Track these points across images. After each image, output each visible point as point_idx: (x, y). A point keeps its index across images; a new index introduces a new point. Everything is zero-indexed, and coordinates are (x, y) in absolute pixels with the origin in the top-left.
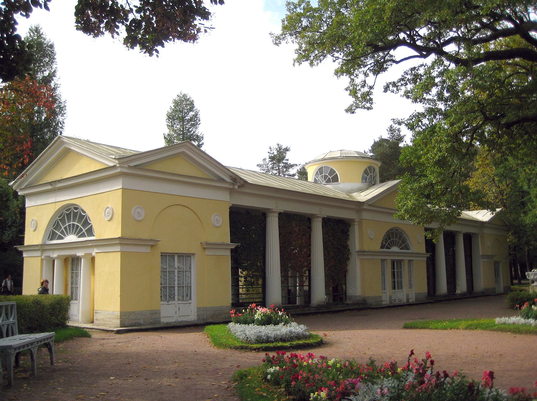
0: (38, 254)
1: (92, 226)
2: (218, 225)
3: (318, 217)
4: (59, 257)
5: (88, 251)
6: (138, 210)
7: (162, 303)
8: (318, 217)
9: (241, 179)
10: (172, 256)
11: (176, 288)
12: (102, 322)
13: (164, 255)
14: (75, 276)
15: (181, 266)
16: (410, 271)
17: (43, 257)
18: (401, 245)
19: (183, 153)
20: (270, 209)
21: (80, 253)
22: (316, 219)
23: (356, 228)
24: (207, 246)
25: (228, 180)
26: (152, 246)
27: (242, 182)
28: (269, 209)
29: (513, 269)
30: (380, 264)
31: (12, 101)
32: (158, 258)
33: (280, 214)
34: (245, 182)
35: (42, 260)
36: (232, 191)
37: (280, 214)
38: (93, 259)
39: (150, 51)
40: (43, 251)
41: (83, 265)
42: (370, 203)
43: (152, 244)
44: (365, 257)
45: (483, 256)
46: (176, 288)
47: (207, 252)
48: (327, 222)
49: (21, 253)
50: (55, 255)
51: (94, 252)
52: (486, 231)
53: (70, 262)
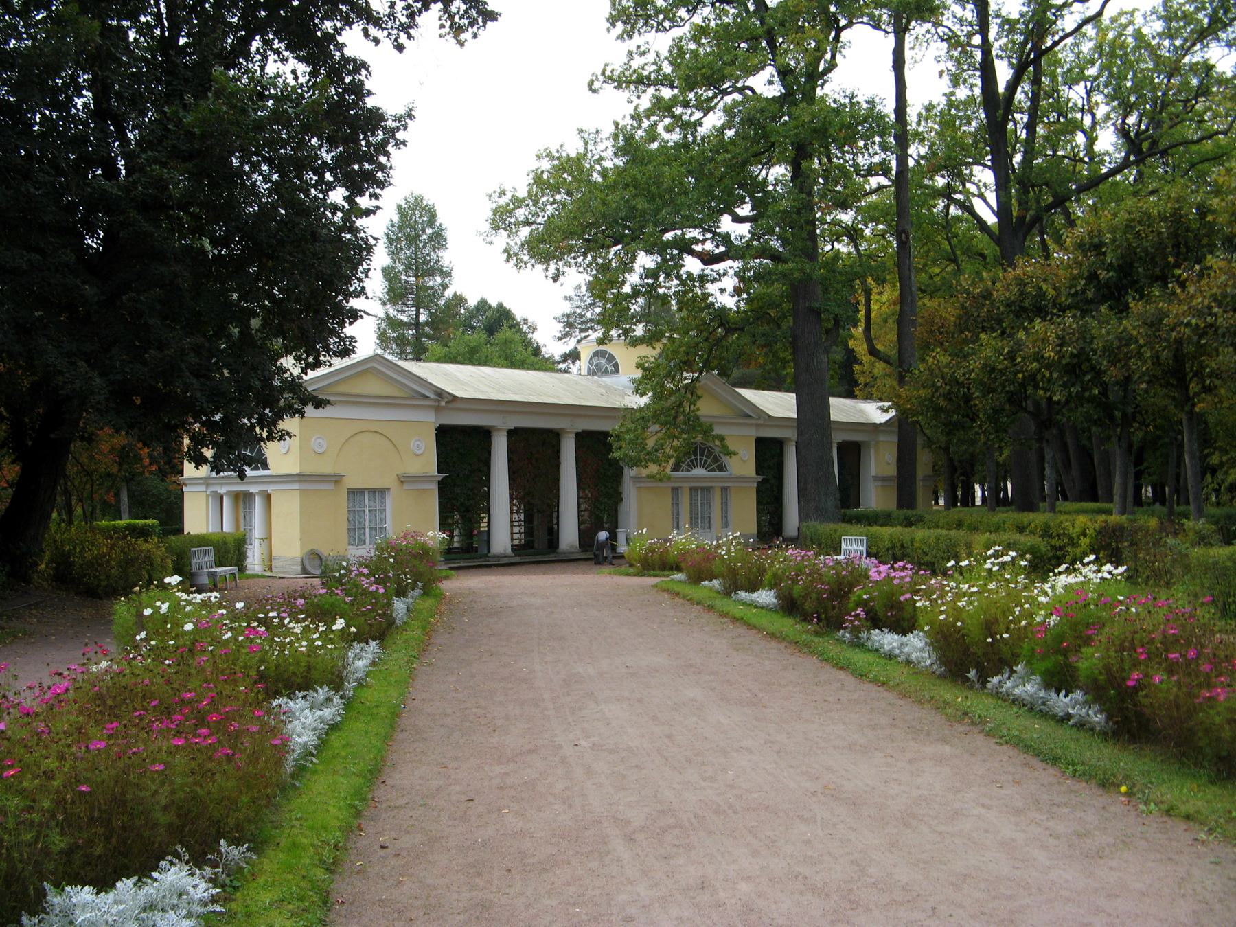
0: (203, 488)
2: (419, 452)
3: (499, 430)
4: (229, 493)
6: (320, 441)
7: (350, 547)
8: (499, 430)
9: (449, 393)
10: (361, 492)
11: (367, 530)
12: (281, 569)
13: (351, 492)
14: (248, 516)
15: (372, 503)
16: (725, 505)
17: (209, 493)
19: (373, 368)
21: (253, 489)
23: (872, 451)
24: (404, 480)
25: (432, 396)
26: (336, 482)
27: (451, 398)
28: (563, 430)
29: (959, 493)
30: (670, 495)
31: (340, 214)
32: (344, 495)
33: (577, 435)
34: (454, 396)
35: (207, 496)
36: (438, 409)
37: (577, 435)
38: (269, 497)
39: (419, 200)
40: (208, 485)
41: (258, 502)
43: (336, 479)
44: (643, 485)
45: (876, 478)
46: (367, 530)
47: (406, 486)
48: (514, 435)
49: (180, 486)
50: (222, 490)
51: (270, 488)
52: (882, 438)
53: (241, 498)
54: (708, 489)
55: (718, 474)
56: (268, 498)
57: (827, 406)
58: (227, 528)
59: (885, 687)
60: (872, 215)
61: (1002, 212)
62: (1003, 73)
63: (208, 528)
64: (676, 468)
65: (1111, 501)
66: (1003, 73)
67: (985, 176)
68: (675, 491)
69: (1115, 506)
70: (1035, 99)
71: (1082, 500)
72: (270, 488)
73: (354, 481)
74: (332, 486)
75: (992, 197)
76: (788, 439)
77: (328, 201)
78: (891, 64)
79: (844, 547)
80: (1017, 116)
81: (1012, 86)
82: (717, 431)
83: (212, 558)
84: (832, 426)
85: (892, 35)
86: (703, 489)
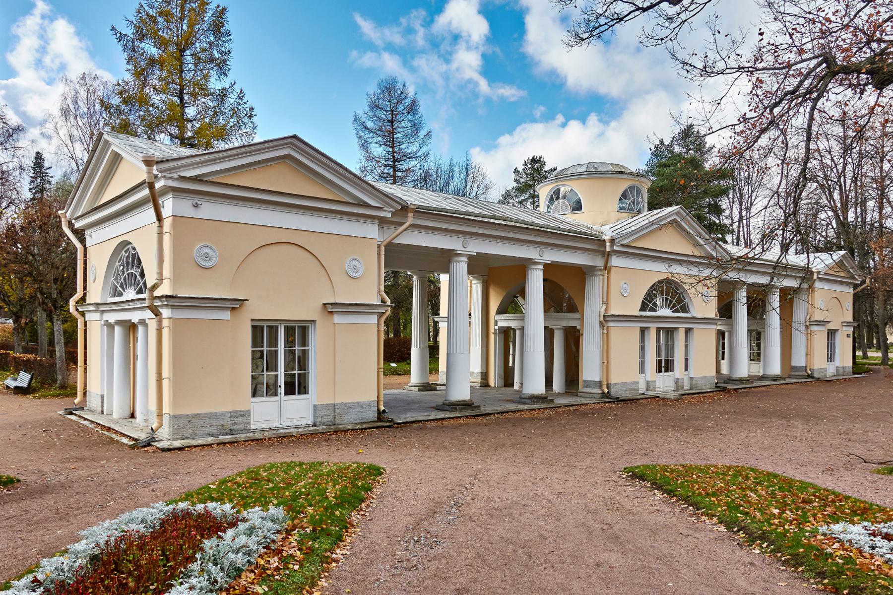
2: (353, 275)
3: (537, 263)
18: (674, 306)
20: (454, 250)
37: (471, 258)
42: (624, 242)
47: (337, 319)
68: (110, 326)
74: (226, 315)
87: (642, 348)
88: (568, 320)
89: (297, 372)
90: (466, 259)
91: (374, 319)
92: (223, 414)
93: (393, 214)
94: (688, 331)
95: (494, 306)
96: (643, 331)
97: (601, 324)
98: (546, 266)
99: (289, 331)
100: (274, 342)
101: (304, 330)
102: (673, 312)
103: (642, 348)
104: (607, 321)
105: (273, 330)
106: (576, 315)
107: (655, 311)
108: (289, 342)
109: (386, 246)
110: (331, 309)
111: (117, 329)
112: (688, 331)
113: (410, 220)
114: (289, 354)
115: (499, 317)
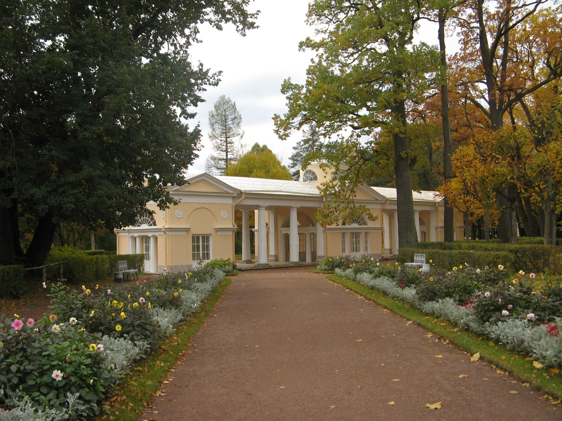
1: (155, 221)
2: (179, 217)
4: (139, 236)
5: (154, 234)
6: (224, 213)
22: (292, 209)
37: (298, 209)
38: (157, 238)
41: (152, 241)
43: (187, 230)
47: (219, 233)
50: (136, 235)
51: (157, 234)
54: (359, 233)
55: (363, 226)
56: (156, 239)
57: (411, 195)
58: (138, 252)
59: (78, 366)
60: (430, 106)
61: (491, 103)
62: (490, 41)
63: (143, 251)
64: (344, 224)
65: (543, 236)
66: (490, 41)
67: (482, 86)
68: (134, 239)
69: (544, 239)
70: (505, 53)
71: (534, 236)
72: (157, 234)
73: (196, 231)
74: (185, 233)
75: (487, 97)
76: (394, 210)
77: (283, 118)
78: (438, 37)
79: (415, 258)
80: (498, 60)
81: (495, 45)
82: (368, 206)
83: (126, 266)
84: (414, 203)
85: (438, 23)
86: (356, 233)
87: (343, 243)
88: (310, 229)
89: (206, 252)
90: (296, 209)
91: (231, 233)
92: (184, 266)
93: (237, 195)
94: (366, 233)
95: (280, 225)
96: (343, 235)
97: (436, 229)
98: (298, 209)
99: (203, 238)
100: (198, 242)
101: (206, 238)
102: (149, 226)
103: (343, 243)
104: (326, 230)
105: (198, 238)
106: (314, 228)
107: (140, 226)
108: (203, 242)
109: (235, 206)
110: (218, 230)
111: (137, 239)
112: (366, 233)
113: (388, 202)
114: (203, 246)
115: (282, 229)
